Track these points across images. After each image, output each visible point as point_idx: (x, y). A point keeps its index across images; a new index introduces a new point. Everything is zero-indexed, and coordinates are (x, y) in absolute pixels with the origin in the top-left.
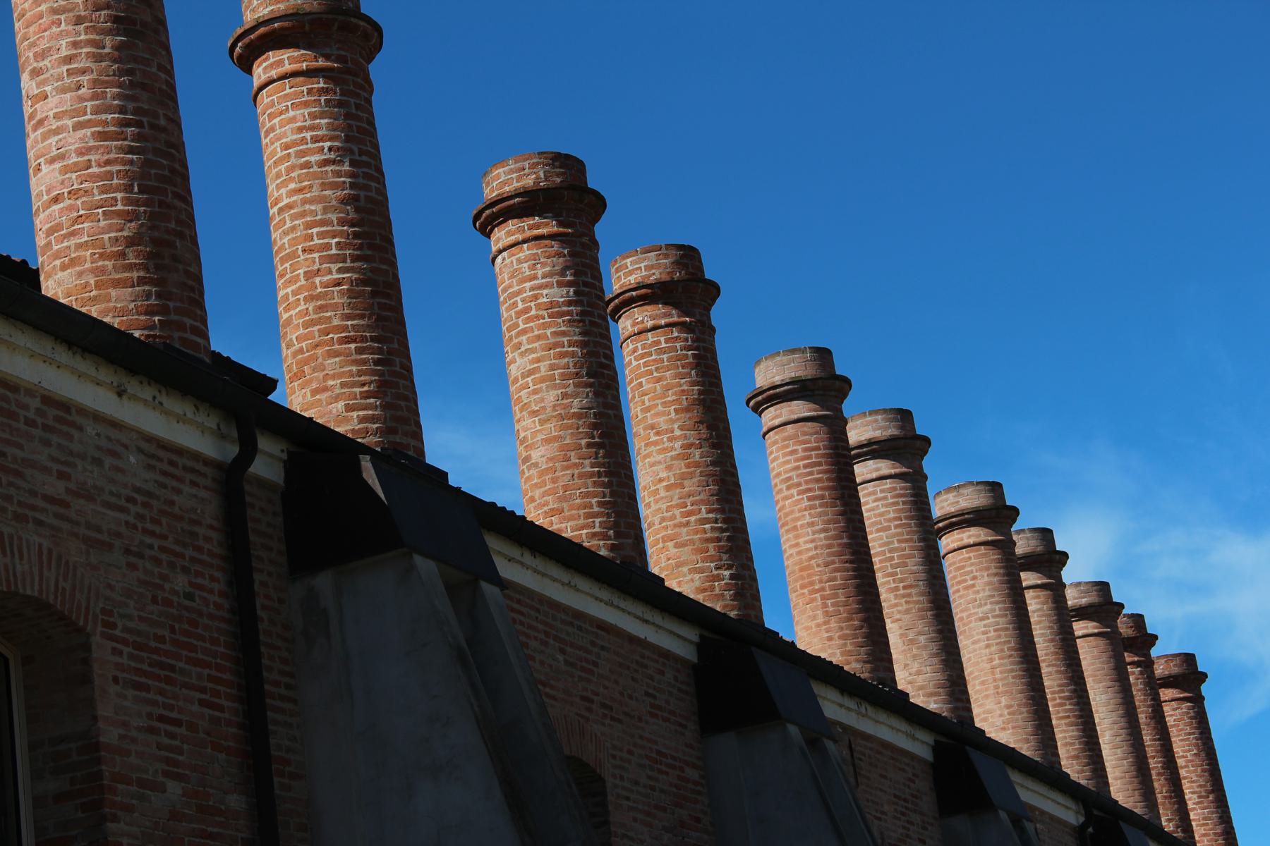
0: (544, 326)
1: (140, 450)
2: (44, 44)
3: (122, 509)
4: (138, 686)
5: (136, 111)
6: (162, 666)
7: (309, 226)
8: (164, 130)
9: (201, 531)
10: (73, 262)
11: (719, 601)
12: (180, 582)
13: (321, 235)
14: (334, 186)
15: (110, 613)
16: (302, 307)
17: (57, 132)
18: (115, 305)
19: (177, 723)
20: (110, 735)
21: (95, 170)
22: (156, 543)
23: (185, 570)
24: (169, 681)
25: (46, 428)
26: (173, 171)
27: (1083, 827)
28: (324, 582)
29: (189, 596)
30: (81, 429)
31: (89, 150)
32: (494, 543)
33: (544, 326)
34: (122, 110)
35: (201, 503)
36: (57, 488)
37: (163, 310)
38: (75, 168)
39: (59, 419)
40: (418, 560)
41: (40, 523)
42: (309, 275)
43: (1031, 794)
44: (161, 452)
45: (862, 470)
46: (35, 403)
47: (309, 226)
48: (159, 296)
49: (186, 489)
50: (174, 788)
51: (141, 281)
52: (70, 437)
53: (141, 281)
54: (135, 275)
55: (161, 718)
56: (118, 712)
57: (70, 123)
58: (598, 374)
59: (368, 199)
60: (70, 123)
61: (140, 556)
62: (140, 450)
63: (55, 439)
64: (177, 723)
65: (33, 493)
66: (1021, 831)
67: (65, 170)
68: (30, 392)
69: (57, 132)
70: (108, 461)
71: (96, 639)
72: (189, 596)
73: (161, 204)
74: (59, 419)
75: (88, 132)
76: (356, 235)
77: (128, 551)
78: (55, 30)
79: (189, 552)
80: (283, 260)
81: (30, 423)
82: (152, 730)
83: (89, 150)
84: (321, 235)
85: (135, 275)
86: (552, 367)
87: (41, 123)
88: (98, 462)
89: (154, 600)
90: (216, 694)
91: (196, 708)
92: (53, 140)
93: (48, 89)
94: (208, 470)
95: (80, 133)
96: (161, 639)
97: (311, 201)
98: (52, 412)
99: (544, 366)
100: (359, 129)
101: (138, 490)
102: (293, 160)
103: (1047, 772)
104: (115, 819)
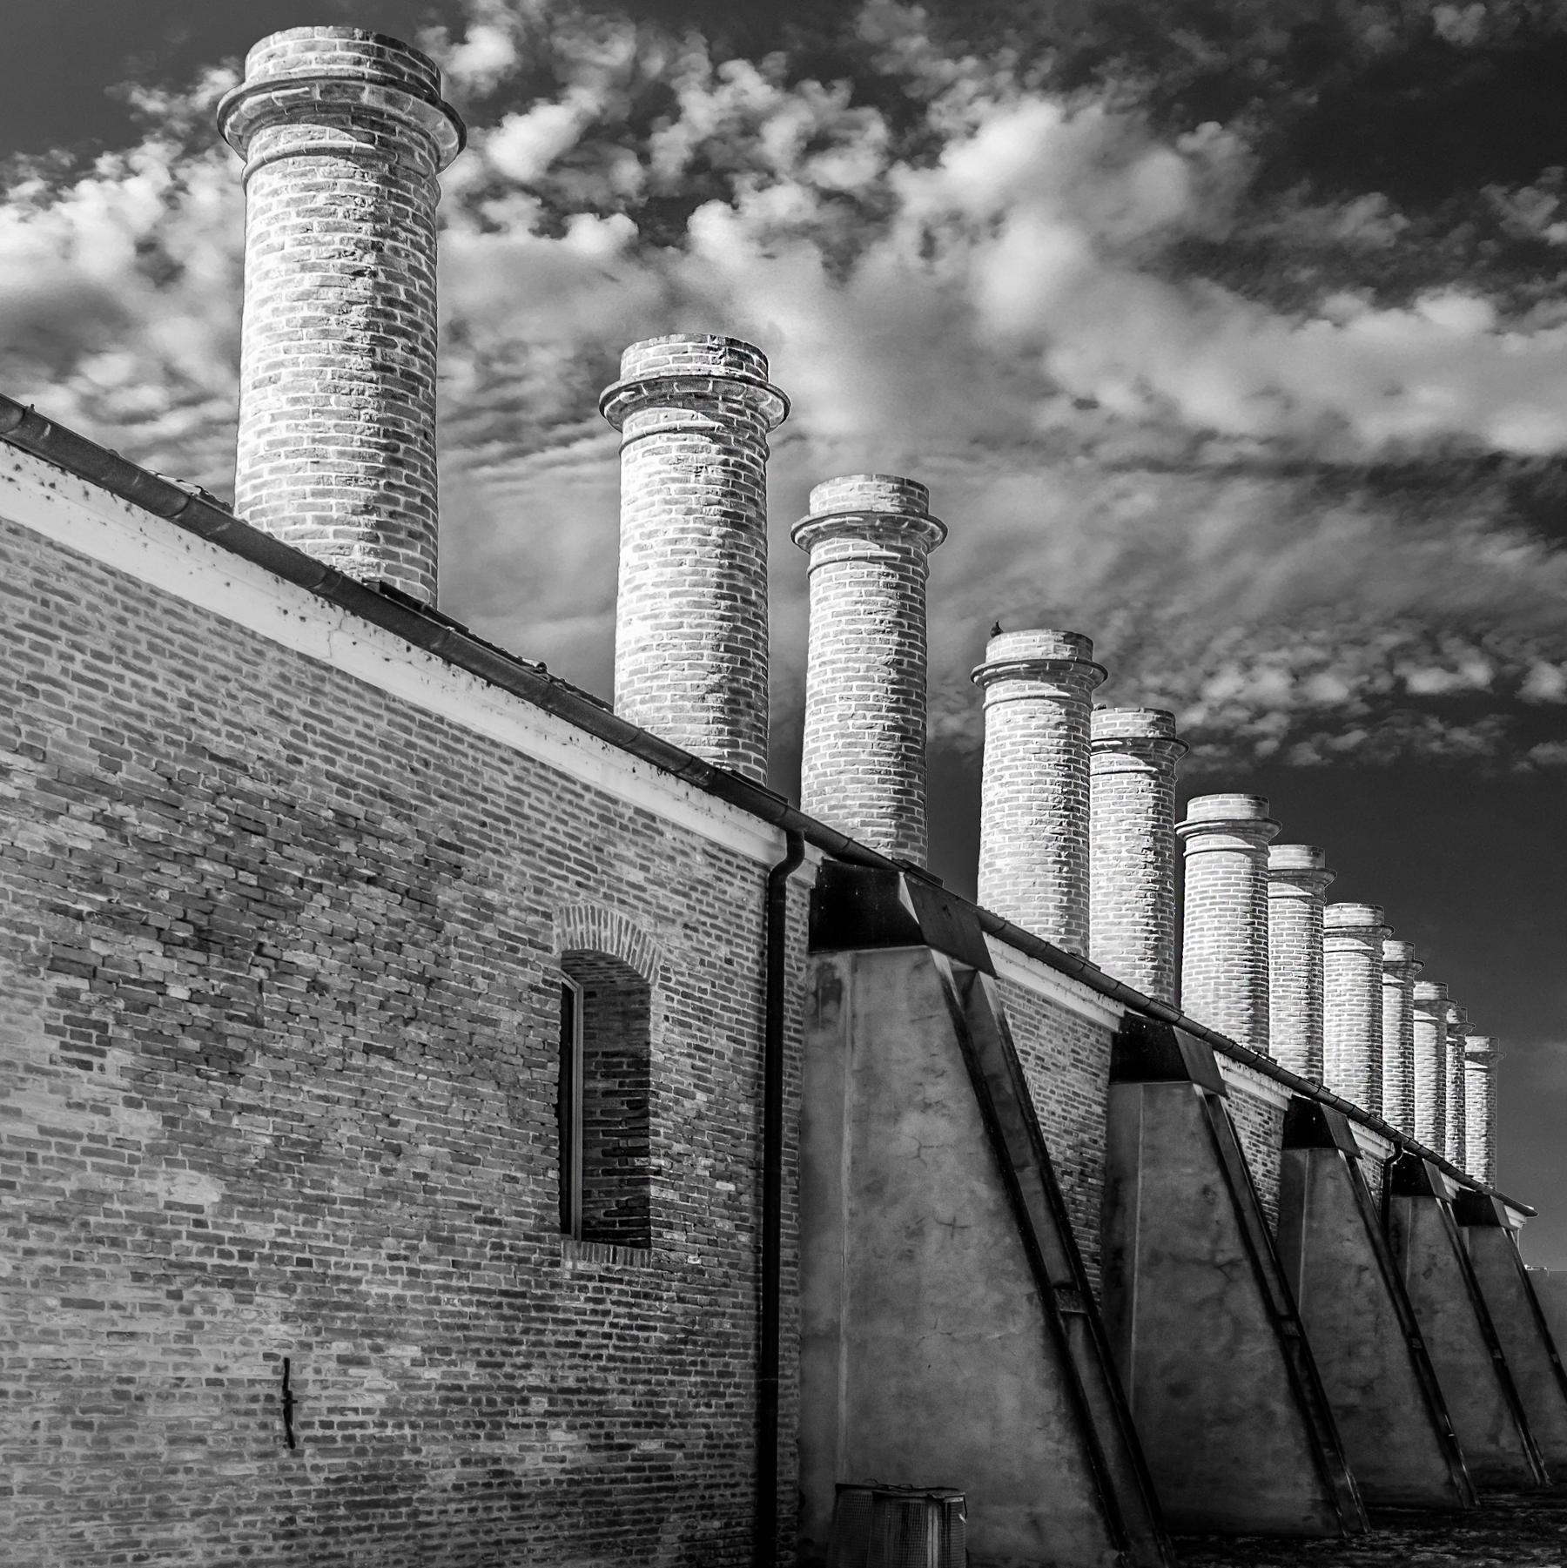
0: (1029, 766)
1: (705, 852)
2: (650, 527)
3: (685, 895)
4: (682, 1024)
5: (731, 587)
6: (702, 1010)
7: (849, 679)
8: (754, 604)
9: (744, 914)
10: (653, 699)
11: (1140, 981)
12: (724, 951)
13: (860, 688)
14: (879, 651)
15: (667, 970)
16: (832, 740)
17: (653, 596)
18: (699, 737)
19: (710, 1052)
20: (657, 1057)
21: (686, 630)
22: (709, 921)
23: (729, 942)
24: (706, 1021)
25: (635, 832)
26: (756, 636)
27: (1390, 1160)
28: (841, 962)
29: (729, 962)
30: (661, 834)
31: (683, 614)
32: (991, 943)
33: (1029, 766)
34: (720, 586)
35: (747, 894)
36: (637, 876)
37: (734, 744)
38: (668, 627)
39: (646, 826)
40: (935, 954)
41: (622, 902)
42: (841, 718)
43: (1235, 1076)
44: (717, 854)
45: (1273, 888)
46: (629, 813)
47: (849, 679)
48: (731, 733)
49: (737, 882)
50: (701, 1097)
51: (716, 720)
52: (652, 838)
53: (716, 720)
54: (711, 715)
55: (698, 1048)
56: (663, 1036)
57: (668, 591)
58: (1074, 807)
59: (911, 664)
60: (668, 591)
61: (695, 930)
62: (705, 852)
63: (641, 840)
64: (710, 1052)
65: (620, 880)
66: (1352, 1164)
67: (658, 627)
68: (626, 805)
69: (653, 596)
70: (680, 859)
71: (655, 989)
72: (729, 962)
73: (743, 662)
74: (646, 826)
75: (684, 600)
76: (894, 692)
77: (686, 926)
78: (665, 517)
79: (733, 929)
80: (817, 703)
81: (623, 828)
82: (690, 1056)
83: (683, 614)
84: (860, 688)
85: (711, 715)
86: (1031, 799)
87: (638, 587)
88: (672, 859)
89: (702, 962)
90: (741, 1033)
91: (724, 1041)
92: (649, 602)
93: (650, 562)
94: (757, 871)
95: (676, 600)
96: (704, 991)
97: (856, 660)
98: (641, 820)
99: (1023, 798)
100: (912, 609)
101: (700, 882)
102: (843, 626)
103: (1371, 1122)
104: (656, 1115)
